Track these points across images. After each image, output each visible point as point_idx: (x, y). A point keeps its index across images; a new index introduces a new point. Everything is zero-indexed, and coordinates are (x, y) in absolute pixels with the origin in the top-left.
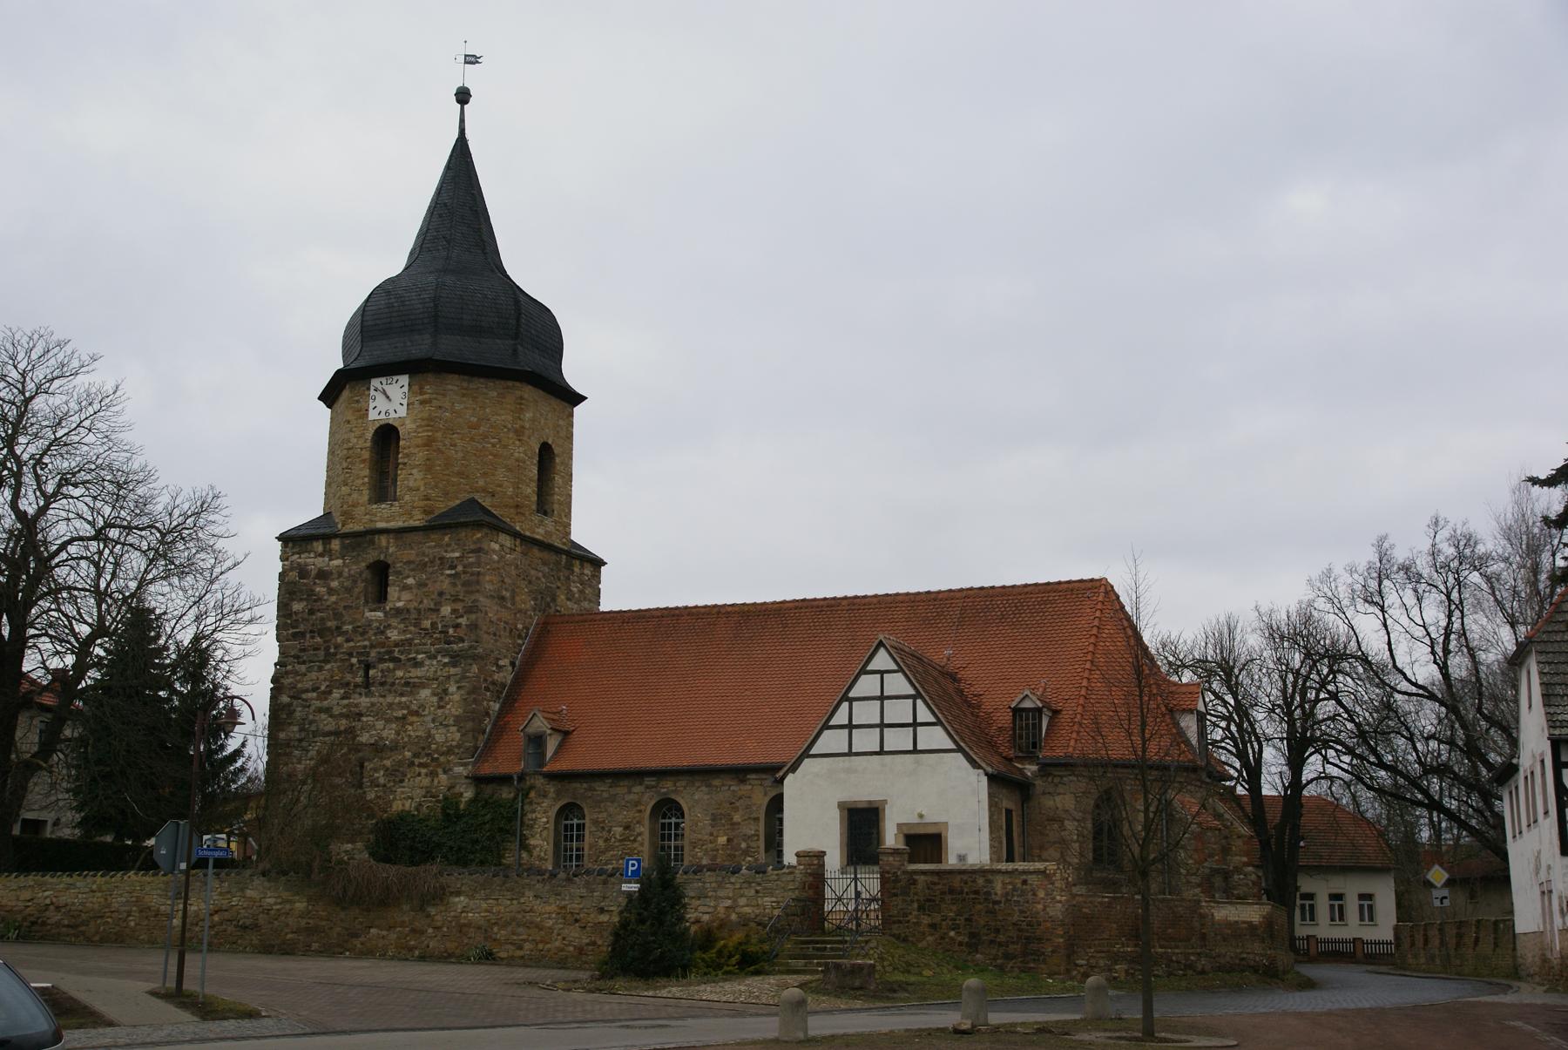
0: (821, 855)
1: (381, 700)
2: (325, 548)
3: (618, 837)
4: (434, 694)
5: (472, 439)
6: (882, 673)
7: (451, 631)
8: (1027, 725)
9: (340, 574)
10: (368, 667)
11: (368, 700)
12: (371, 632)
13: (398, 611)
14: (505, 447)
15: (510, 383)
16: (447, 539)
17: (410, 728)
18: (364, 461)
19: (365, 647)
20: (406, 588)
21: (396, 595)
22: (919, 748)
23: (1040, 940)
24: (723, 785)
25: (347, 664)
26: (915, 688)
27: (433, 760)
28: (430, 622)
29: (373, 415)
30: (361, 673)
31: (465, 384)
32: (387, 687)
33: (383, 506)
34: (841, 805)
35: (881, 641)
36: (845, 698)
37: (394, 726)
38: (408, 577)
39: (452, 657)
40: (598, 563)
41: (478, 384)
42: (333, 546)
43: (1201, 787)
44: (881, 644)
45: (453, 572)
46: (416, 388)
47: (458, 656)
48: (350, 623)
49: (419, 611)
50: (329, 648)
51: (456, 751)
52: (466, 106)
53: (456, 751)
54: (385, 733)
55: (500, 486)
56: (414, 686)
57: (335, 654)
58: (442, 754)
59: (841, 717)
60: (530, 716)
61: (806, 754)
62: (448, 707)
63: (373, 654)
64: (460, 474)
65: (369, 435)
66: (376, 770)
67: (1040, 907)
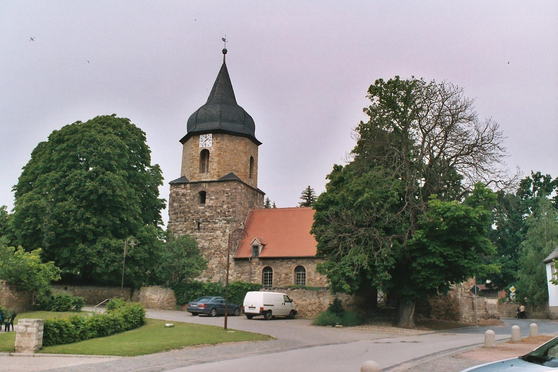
5: (232, 154)
7: (227, 213)
9: (190, 195)
10: (199, 224)
13: (209, 207)
18: (198, 160)
20: (211, 199)
21: (208, 201)
29: (200, 146)
30: (197, 225)
40: (263, 194)
49: (216, 207)
63: (201, 219)
64: (228, 165)
65: (200, 151)
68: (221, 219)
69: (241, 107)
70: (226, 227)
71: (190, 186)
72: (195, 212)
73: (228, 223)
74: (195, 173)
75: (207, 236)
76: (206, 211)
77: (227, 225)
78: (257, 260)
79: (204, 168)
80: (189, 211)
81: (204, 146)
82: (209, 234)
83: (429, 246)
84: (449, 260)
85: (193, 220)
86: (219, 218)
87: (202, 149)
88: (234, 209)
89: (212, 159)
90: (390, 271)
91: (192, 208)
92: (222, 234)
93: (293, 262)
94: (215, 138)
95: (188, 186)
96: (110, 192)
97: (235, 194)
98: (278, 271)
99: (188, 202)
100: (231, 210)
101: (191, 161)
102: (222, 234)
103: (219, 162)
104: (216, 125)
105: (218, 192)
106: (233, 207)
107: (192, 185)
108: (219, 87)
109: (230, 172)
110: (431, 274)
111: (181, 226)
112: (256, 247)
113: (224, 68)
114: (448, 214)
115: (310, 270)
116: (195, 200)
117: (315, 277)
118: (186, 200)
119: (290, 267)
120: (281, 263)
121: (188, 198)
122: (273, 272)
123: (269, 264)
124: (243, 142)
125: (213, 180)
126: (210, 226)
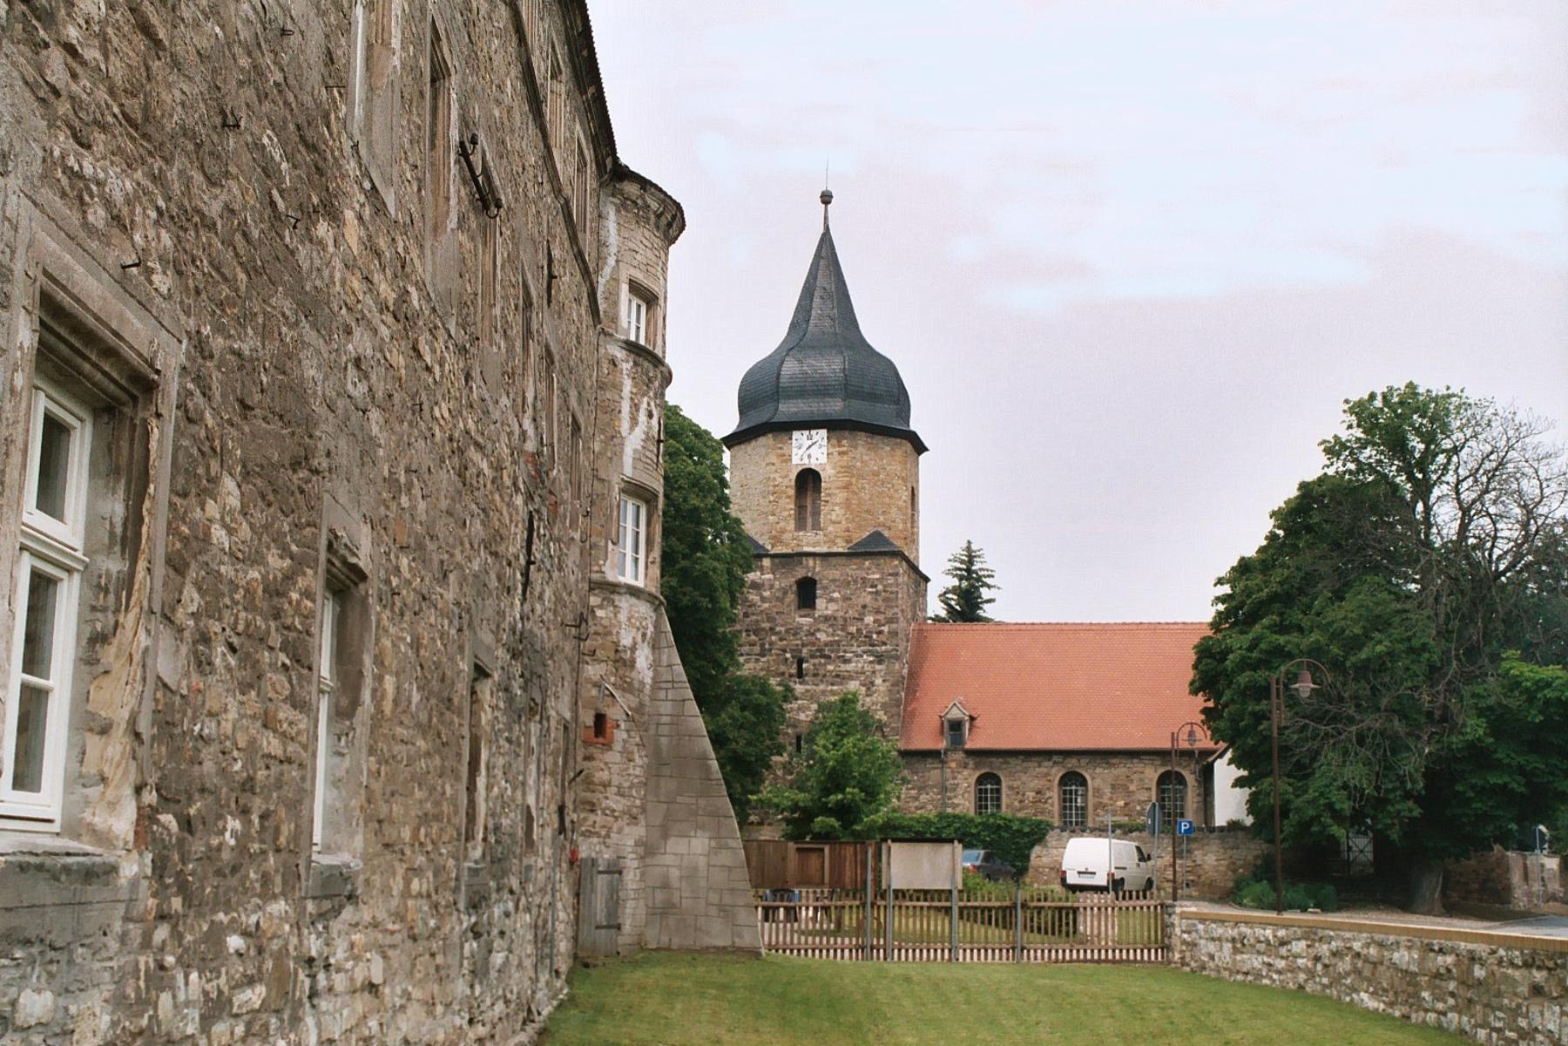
7: (875, 636)
9: (772, 587)
10: (800, 662)
13: (826, 619)
14: (896, 491)
18: (789, 497)
20: (832, 600)
29: (795, 460)
30: (795, 666)
41: (877, 439)
49: (845, 620)
63: (805, 650)
64: (868, 511)
65: (793, 476)
68: (859, 650)
69: (884, 358)
70: (874, 672)
71: (772, 563)
72: (787, 631)
73: (880, 663)
74: (783, 531)
75: (823, 692)
76: (819, 630)
77: (878, 667)
78: (960, 756)
79: (805, 518)
80: (772, 629)
81: (806, 461)
82: (830, 688)
83: (1495, 752)
84: (1536, 780)
85: (785, 651)
86: (854, 649)
87: (800, 469)
88: (894, 626)
89: (829, 495)
90: (1419, 800)
91: (779, 621)
92: (864, 689)
93: (1055, 763)
94: (834, 441)
95: (766, 562)
96: (705, 602)
97: (894, 589)
98: (1015, 784)
99: (766, 605)
100: (885, 629)
101: (772, 498)
102: (864, 689)
103: (847, 505)
104: (835, 407)
105: (849, 583)
106: (890, 621)
107: (777, 560)
108: (822, 297)
109: (872, 530)
110: (1492, 807)
111: (751, 665)
112: (956, 726)
113: (826, 241)
114: (1549, 693)
115: (1098, 782)
116: (787, 600)
117: (1111, 799)
118: (763, 599)
119: (1047, 774)
120: (1025, 764)
121: (767, 594)
122: (1004, 784)
123: (995, 765)
124: (899, 452)
125: (835, 550)
126: (830, 667)
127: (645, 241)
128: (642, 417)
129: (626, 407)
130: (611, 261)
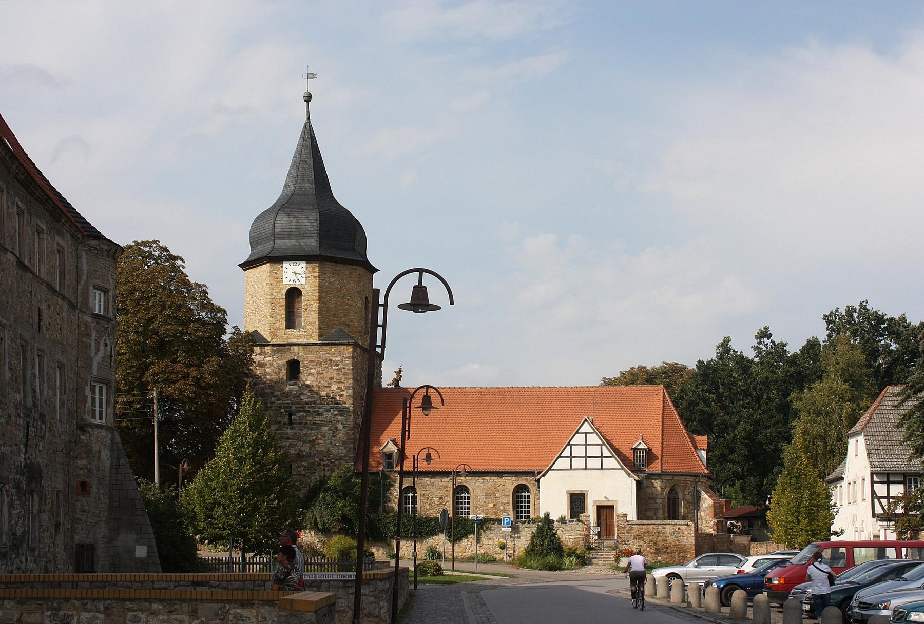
0: (564, 517)
1: (300, 431)
2: (261, 351)
3: (436, 502)
4: (330, 430)
6: (586, 433)
8: (640, 456)
9: (272, 365)
10: (291, 415)
11: (292, 431)
12: (291, 396)
14: (354, 301)
15: (354, 267)
16: (333, 350)
17: (318, 446)
18: (282, 306)
19: (288, 404)
20: (310, 374)
22: (603, 468)
23: (685, 551)
24: (491, 479)
25: (278, 412)
26: (602, 440)
27: (331, 462)
28: (325, 392)
29: (285, 281)
30: (287, 417)
31: (334, 268)
32: (303, 425)
33: (295, 331)
34: (567, 492)
35: (586, 419)
36: (569, 444)
37: (308, 445)
38: (312, 369)
39: (339, 411)
41: (340, 267)
42: (266, 350)
43: (32, 318)
44: (586, 420)
45: (337, 367)
46: (310, 269)
47: (343, 410)
48: (278, 391)
50: (267, 403)
51: (344, 459)
52: (309, 103)
53: (344, 459)
54: (303, 449)
55: (352, 321)
56: (318, 425)
57: (271, 407)
58: (337, 460)
59: (567, 452)
60: (386, 443)
61: (550, 469)
62: (338, 436)
63: (294, 407)
64: (334, 315)
65: (284, 292)
66: (298, 467)
67: (685, 538)
82: (309, 432)
125: (312, 341)
127: (101, 265)
128: (102, 347)
129: (93, 344)
130: (84, 277)
